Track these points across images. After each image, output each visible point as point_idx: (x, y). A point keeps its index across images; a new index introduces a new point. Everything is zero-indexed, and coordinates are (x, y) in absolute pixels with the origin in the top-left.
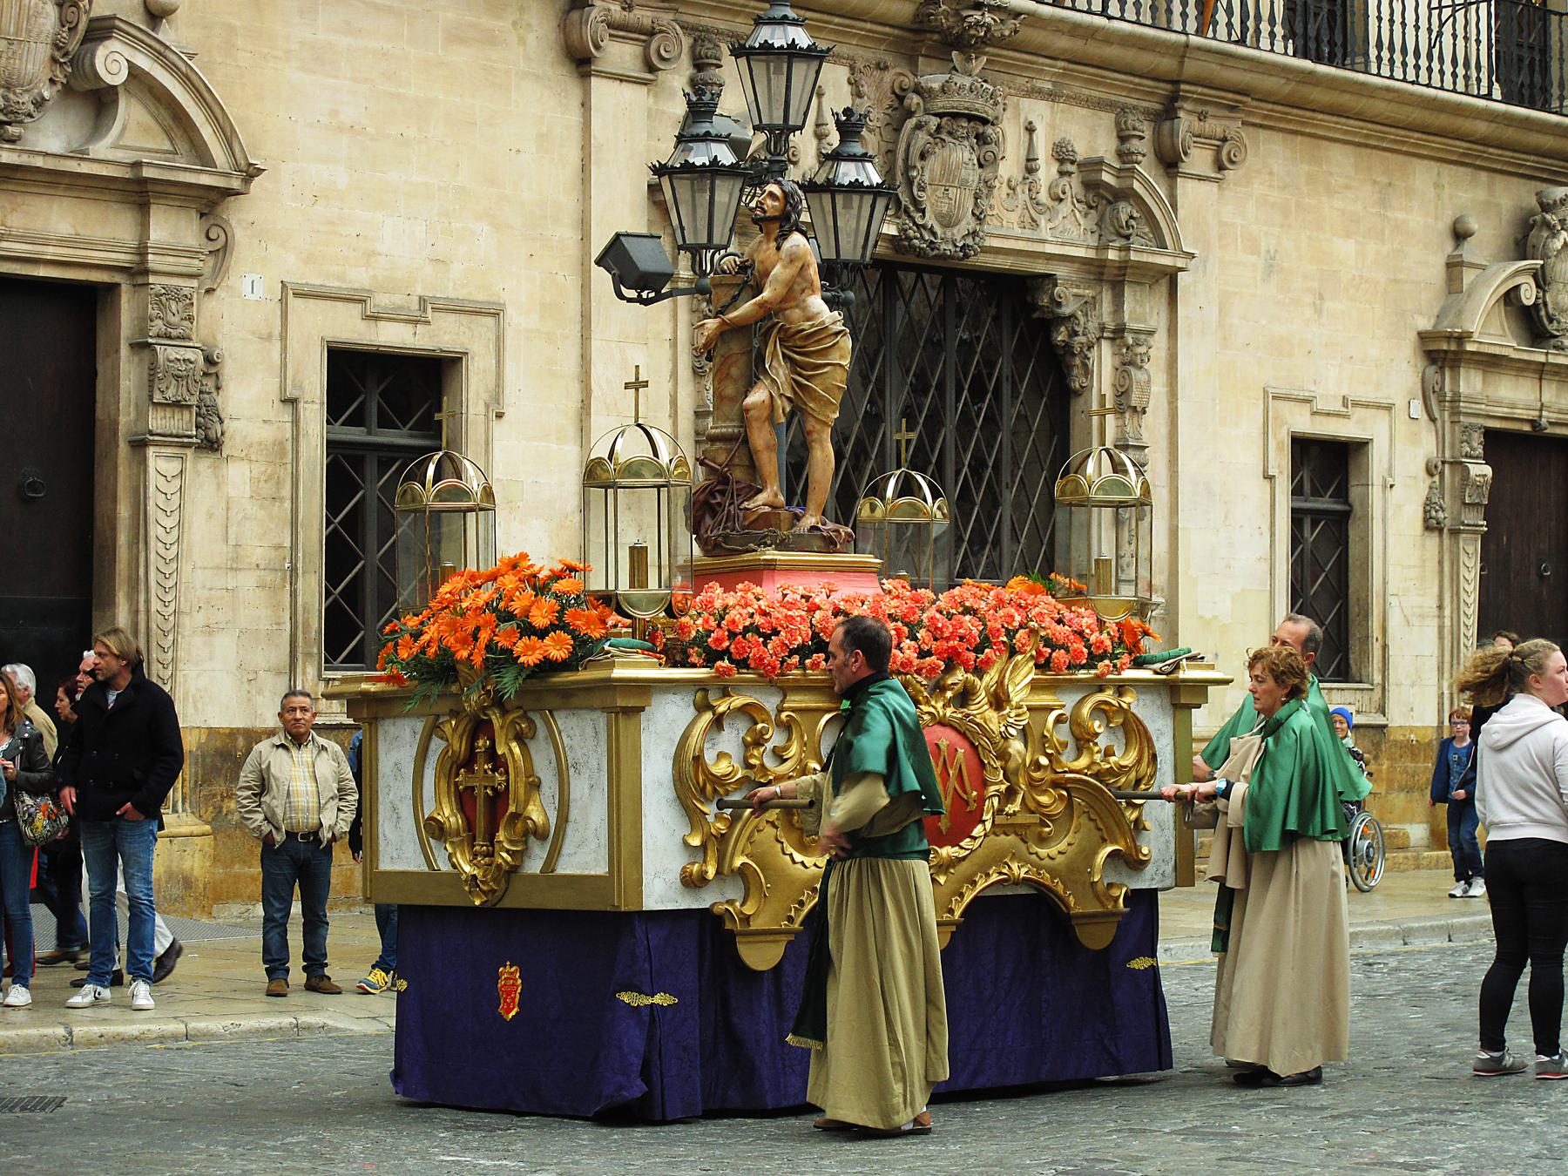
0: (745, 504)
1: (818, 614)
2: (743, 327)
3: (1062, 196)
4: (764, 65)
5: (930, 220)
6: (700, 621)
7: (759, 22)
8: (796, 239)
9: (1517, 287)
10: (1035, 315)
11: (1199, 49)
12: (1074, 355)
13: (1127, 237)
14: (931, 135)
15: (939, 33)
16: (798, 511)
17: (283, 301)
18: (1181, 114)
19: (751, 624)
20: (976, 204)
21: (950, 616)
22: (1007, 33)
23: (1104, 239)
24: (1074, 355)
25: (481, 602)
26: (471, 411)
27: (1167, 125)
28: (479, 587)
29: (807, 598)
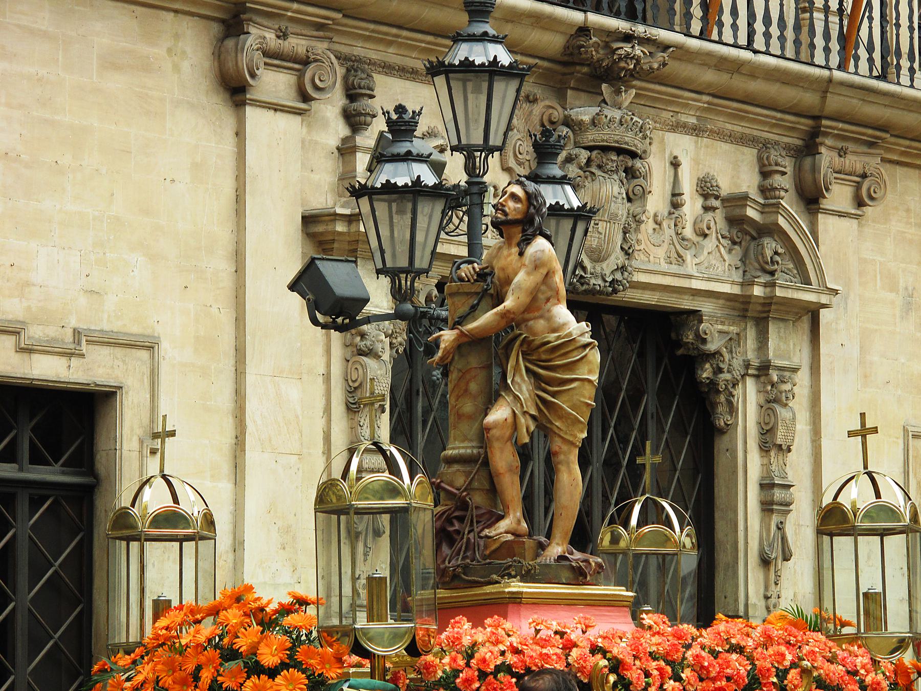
0: (486, 532)
1: (575, 653)
2: (484, 339)
3: (707, 232)
4: (460, 84)
6: (446, 660)
7: (458, 38)
8: (540, 244)
10: (680, 352)
11: (842, 84)
12: (718, 392)
13: (772, 273)
14: (581, 168)
15: (589, 65)
16: (543, 539)
18: (823, 150)
19: (503, 663)
20: (625, 239)
21: (714, 654)
22: (656, 66)
23: (748, 276)
24: (718, 392)
25: (202, 639)
26: (125, 447)
27: (808, 161)
28: (198, 622)
29: (561, 634)
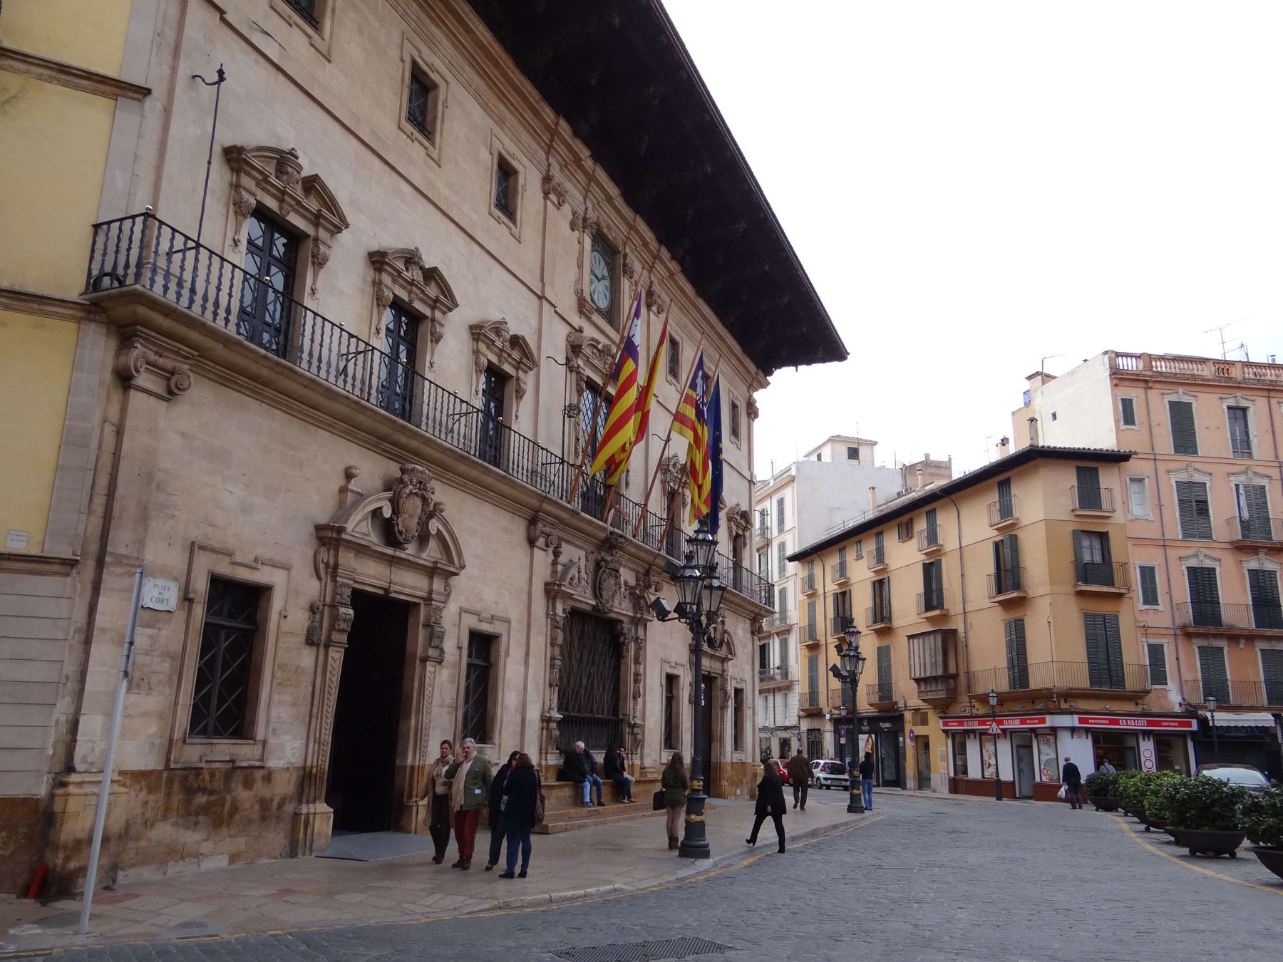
5: (604, 602)
17: (460, 614)
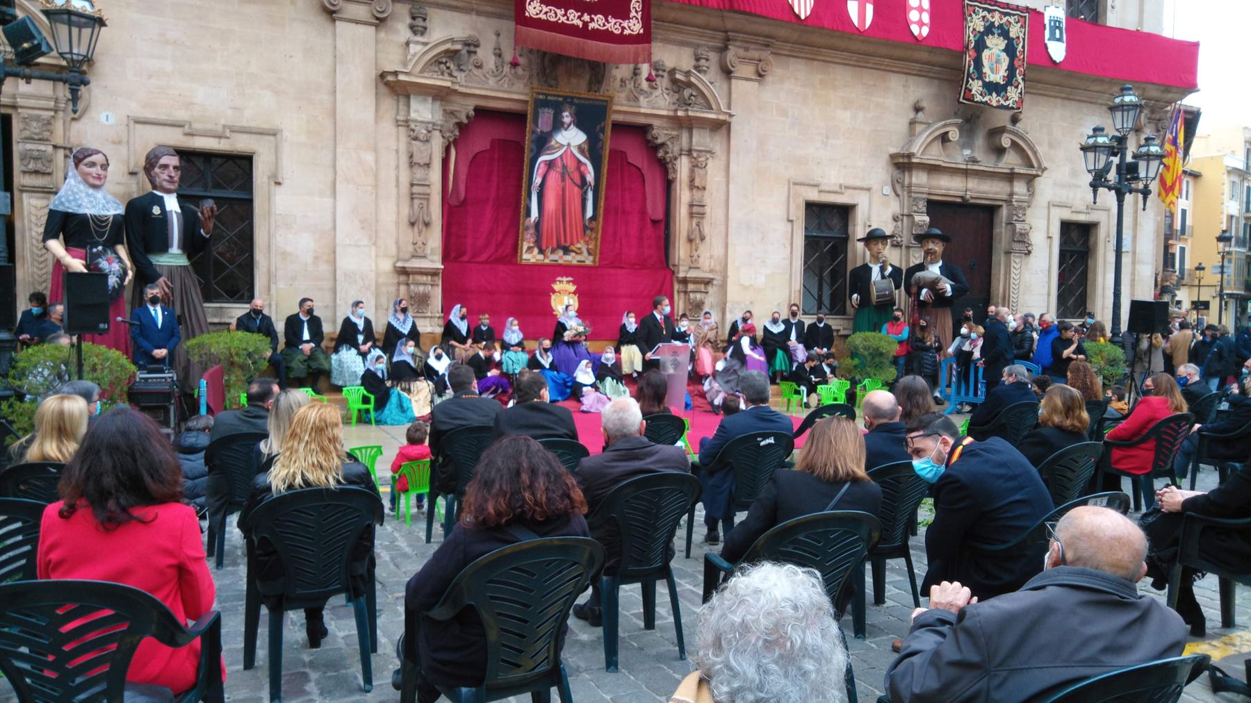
9: (947, 133)
17: (1049, 208)
